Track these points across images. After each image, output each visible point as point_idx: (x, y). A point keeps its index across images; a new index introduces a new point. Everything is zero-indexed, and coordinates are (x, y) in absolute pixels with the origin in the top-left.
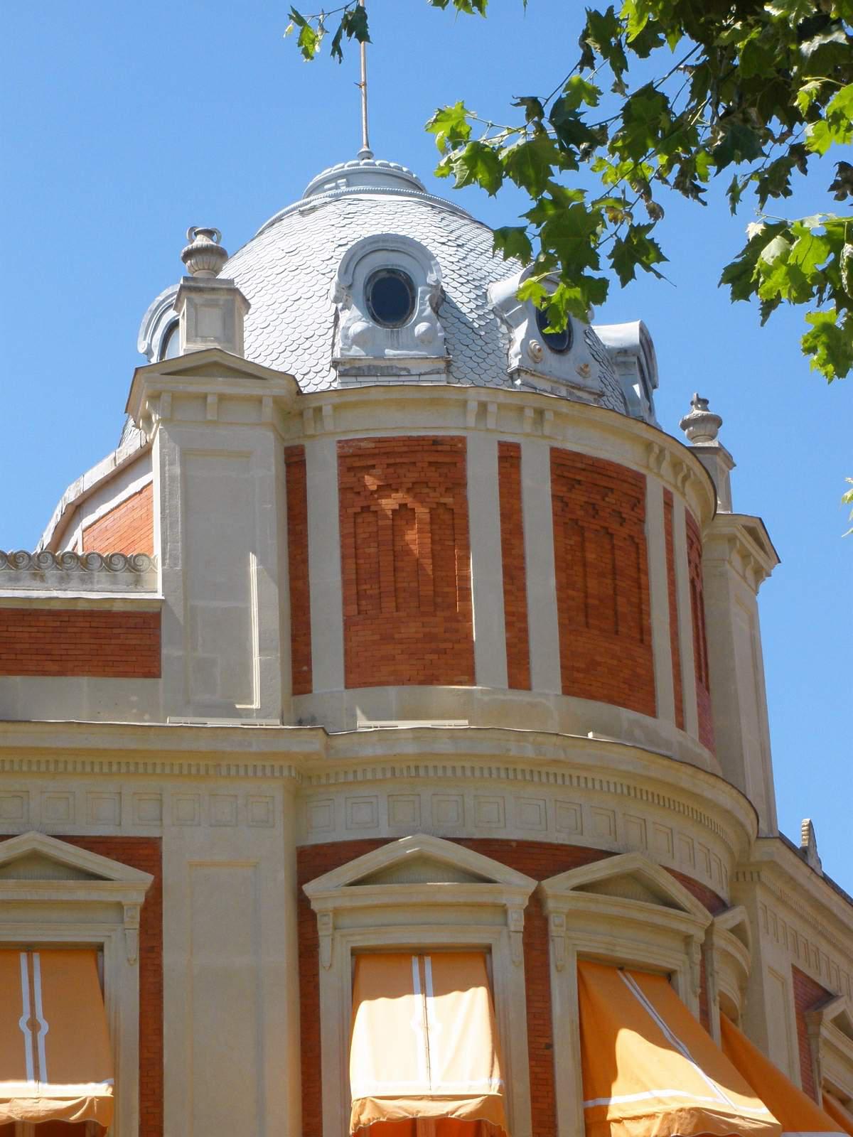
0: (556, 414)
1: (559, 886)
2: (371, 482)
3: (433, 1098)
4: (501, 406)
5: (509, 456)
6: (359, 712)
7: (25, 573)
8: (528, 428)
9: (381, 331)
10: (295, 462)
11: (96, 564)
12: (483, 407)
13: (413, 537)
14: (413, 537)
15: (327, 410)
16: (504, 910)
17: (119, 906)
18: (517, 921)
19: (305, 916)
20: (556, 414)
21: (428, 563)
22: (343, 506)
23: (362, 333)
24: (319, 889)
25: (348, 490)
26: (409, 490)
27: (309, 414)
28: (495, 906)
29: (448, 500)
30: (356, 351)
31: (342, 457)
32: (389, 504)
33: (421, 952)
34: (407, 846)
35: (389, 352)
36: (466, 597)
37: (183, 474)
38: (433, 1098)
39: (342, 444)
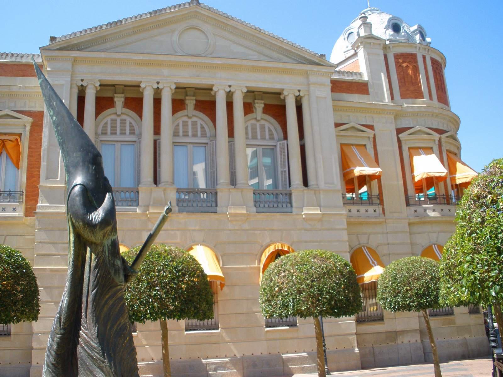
0: (431, 50)
1: (443, 136)
2: (401, 61)
3: (437, 173)
4: (423, 48)
5: (424, 57)
6: (404, 103)
7: (341, 75)
8: (426, 52)
9: (396, 34)
10: (386, 57)
11: (354, 74)
12: (420, 48)
13: (410, 71)
14: (410, 71)
15: (391, 47)
16: (434, 141)
17: (369, 137)
18: (437, 143)
19: (399, 141)
20: (431, 50)
21: (413, 76)
22: (396, 65)
23: (392, 34)
24: (402, 136)
25: (397, 63)
26: (408, 63)
27: (387, 48)
28: (433, 140)
29: (415, 65)
30: (391, 38)
31: (394, 56)
32: (405, 65)
33: (420, 148)
34: (417, 128)
35: (398, 38)
36: (420, 83)
37: (368, 57)
38: (437, 173)
39: (394, 54)
